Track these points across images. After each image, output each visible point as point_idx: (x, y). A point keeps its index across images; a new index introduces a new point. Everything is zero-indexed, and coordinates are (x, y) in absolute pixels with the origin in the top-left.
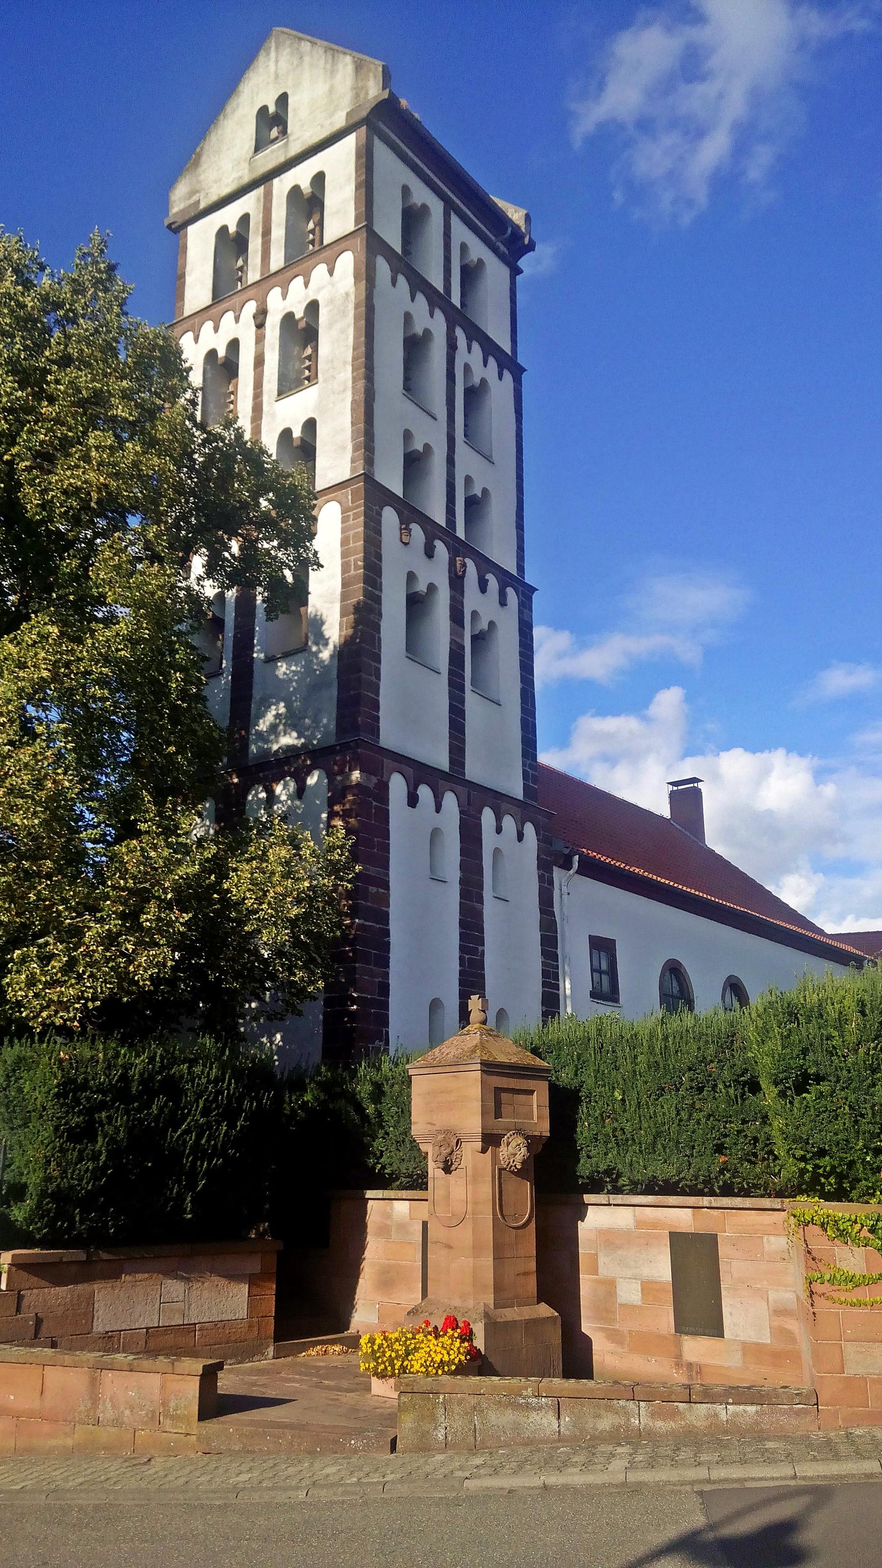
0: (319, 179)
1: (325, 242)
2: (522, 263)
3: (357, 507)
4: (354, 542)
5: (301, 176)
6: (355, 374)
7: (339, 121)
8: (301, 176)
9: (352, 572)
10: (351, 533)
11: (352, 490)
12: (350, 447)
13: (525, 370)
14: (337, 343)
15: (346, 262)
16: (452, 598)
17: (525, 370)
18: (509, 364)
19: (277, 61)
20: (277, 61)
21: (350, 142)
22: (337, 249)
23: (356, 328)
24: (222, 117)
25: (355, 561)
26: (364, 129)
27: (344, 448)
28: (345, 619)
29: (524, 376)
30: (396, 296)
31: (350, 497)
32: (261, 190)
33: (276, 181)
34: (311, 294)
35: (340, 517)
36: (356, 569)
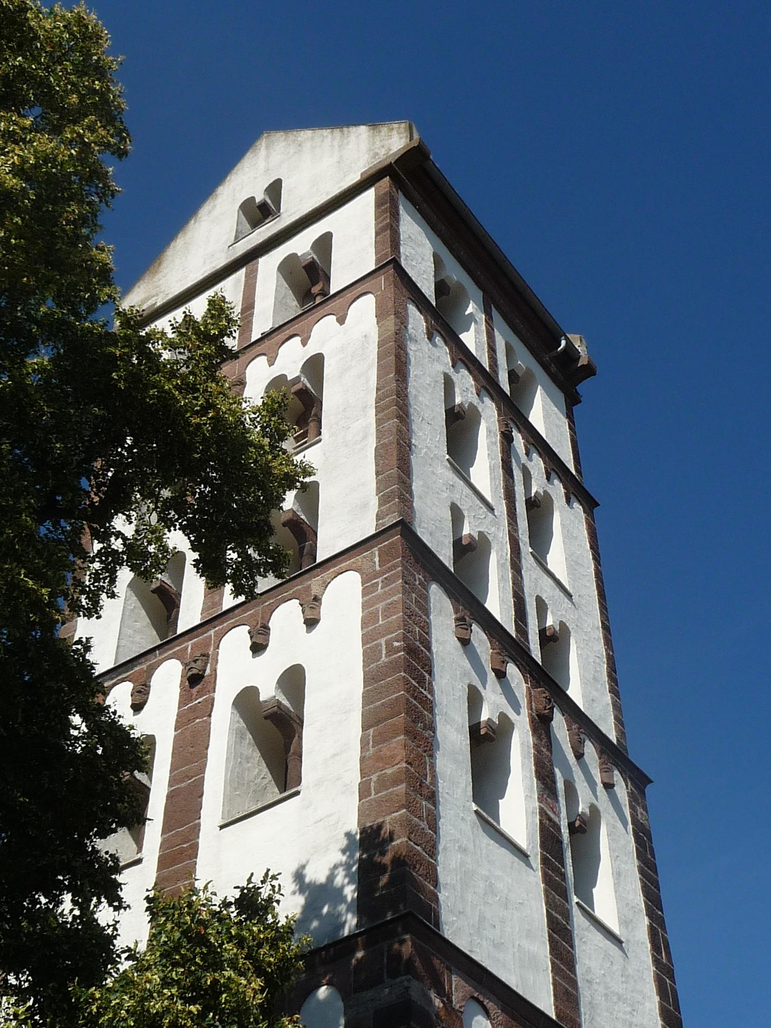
0: (315, 366)
1: (333, 291)
2: (582, 388)
3: (390, 569)
4: (385, 617)
5: (301, 245)
6: (381, 415)
7: (354, 178)
8: (301, 245)
9: (381, 622)
10: (380, 606)
11: (379, 549)
12: (374, 502)
13: (651, 781)
14: (334, 737)
15: (364, 310)
16: (516, 531)
17: (651, 781)
18: (577, 491)
19: (267, 157)
20: (267, 157)
21: (369, 196)
22: (349, 295)
23: (380, 434)
24: (193, 221)
25: (389, 644)
26: (386, 181)
27: (354, 793)
28: (371, 731)
29: (649, 789)
30: (429, 361)
31: (377, 559)
32: (242, 272)
33: (262, 260)
34: (312, 349)
35: (361, 588)
36: (391, 650)
